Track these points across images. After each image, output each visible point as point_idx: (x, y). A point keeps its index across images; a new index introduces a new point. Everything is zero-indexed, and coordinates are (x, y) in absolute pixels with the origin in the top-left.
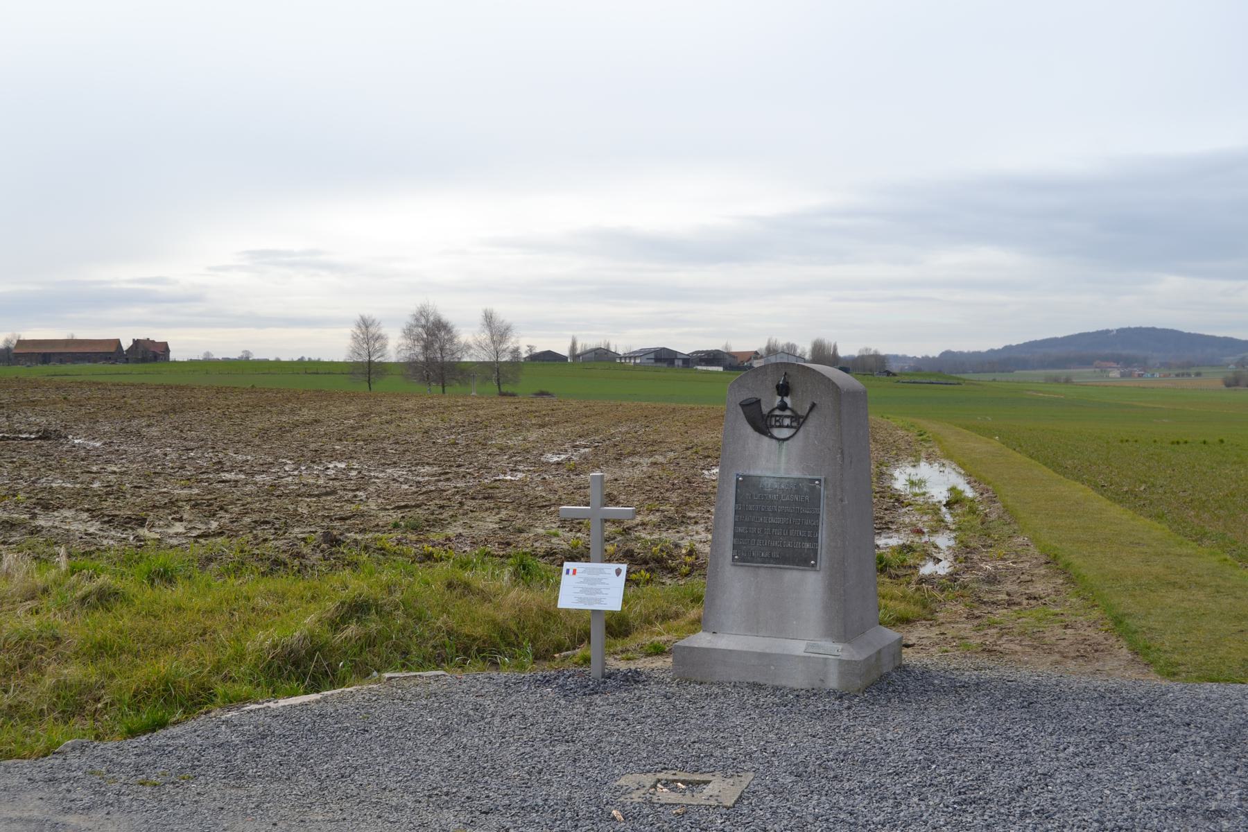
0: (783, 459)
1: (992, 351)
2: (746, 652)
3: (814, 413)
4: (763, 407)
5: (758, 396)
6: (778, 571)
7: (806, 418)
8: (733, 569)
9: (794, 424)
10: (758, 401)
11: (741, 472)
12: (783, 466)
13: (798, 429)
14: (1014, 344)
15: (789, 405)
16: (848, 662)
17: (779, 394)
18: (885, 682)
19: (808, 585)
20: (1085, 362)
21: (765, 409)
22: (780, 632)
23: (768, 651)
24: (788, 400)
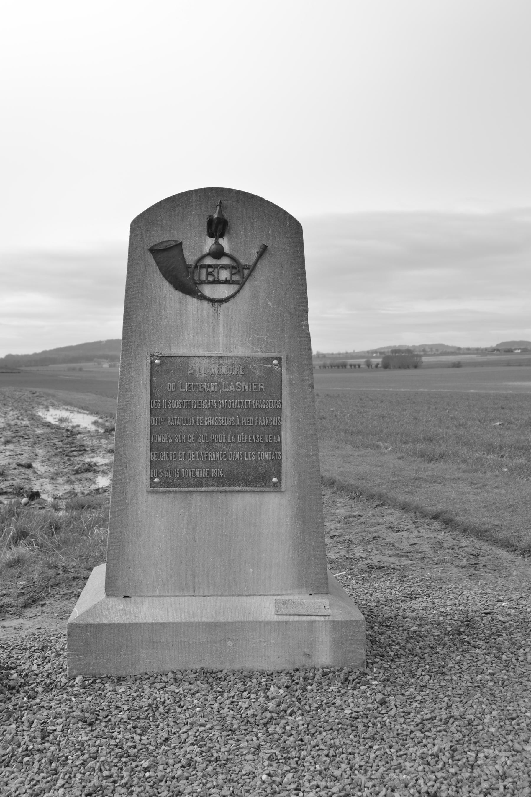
0: (221, 330)
1: (35, 354)
2: (188, 625)
3: (264, 262)
4: (186, 253)
5: (177, 237)
6: (221, 496)
7: (252, 269)
9: (236, 278)
10: (179, 245)
11: (156, 351)
12: (221, 340)
13: (241, 285)
14: (48, 349)
15: (227, 250)
16: (346, 624)
17: (211, 235)
18: (385, 645)
19: (271, 512)
20: (89, 359)
21: (190, 258)
22: (230, 585)
23: (220, 619)
24: (224, 242)
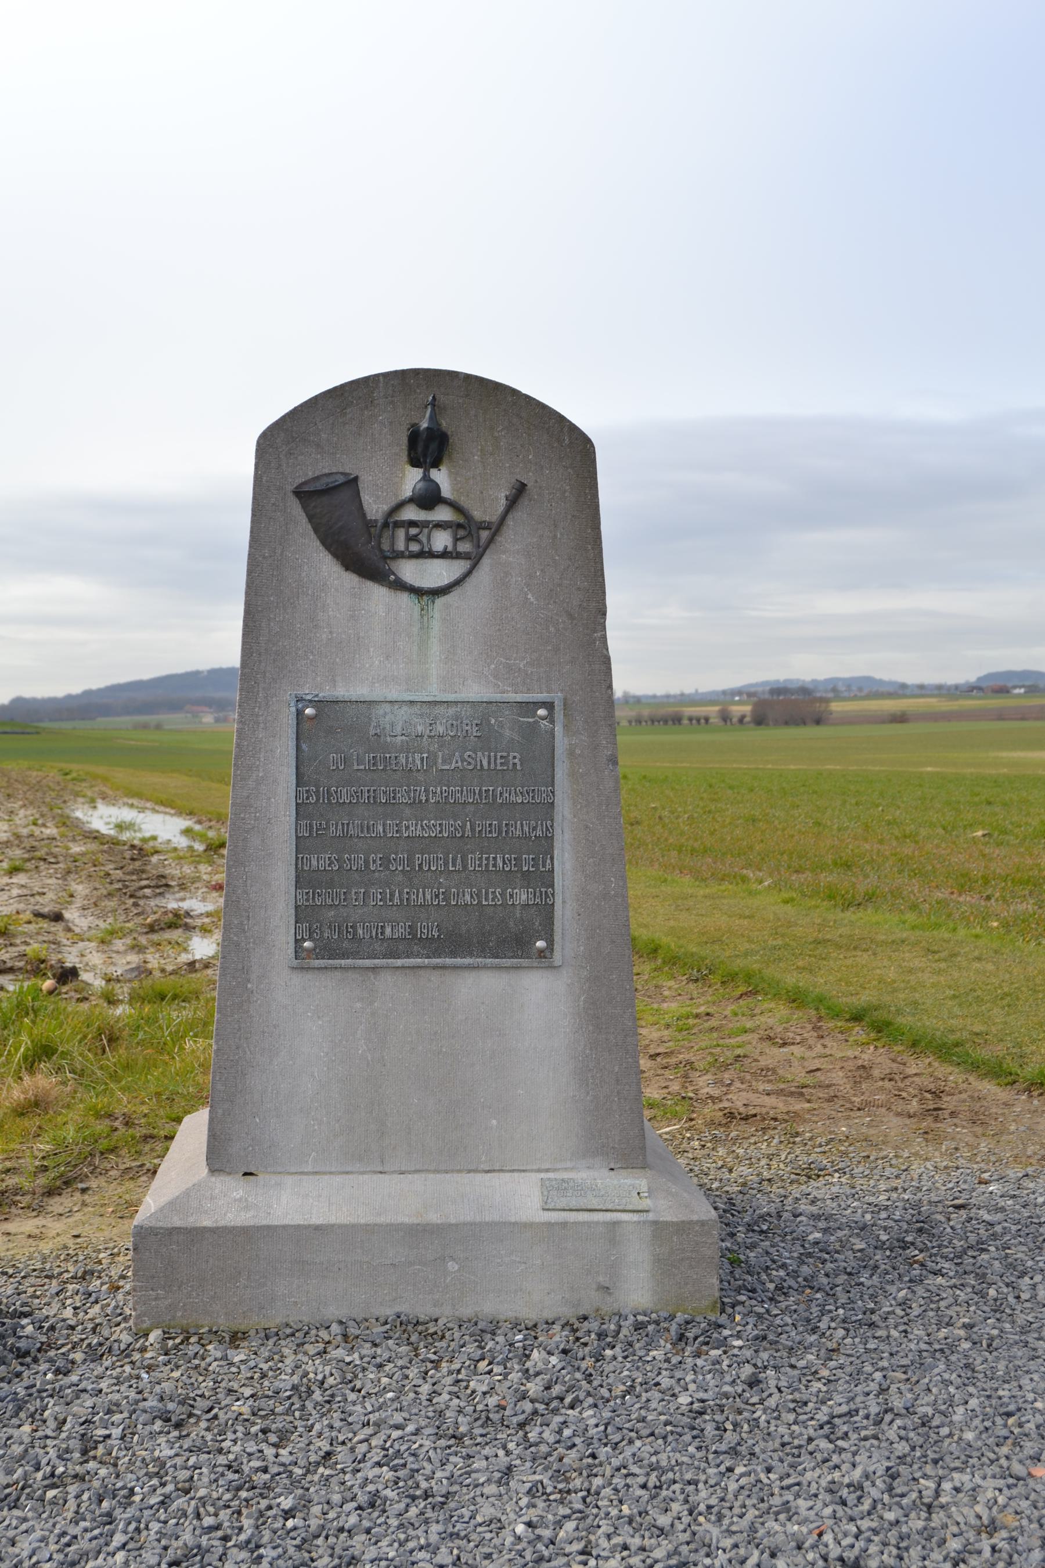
0: (435, 649)
1: (69, 697)
2: (370, 1229)
3: (519, 514)
4: (366, 499)
5: (350, 467)
6: (435, 977)
7: (497, 528)
8: (297, 980)
9: (464, 547)
10: (353, 482)
11: (307, 691)
12: (435, 668)
13: (475, 560)
14: (94, 687)
15: (446, 491)
16: (682, 1228)
17: (414, 463)
18: (757, 1269)
19: (534, 1007)
20: (175, 706)
21: (375, 507)
22: (453, 1152)
23: (434, 1218)
24: (441, 477)
